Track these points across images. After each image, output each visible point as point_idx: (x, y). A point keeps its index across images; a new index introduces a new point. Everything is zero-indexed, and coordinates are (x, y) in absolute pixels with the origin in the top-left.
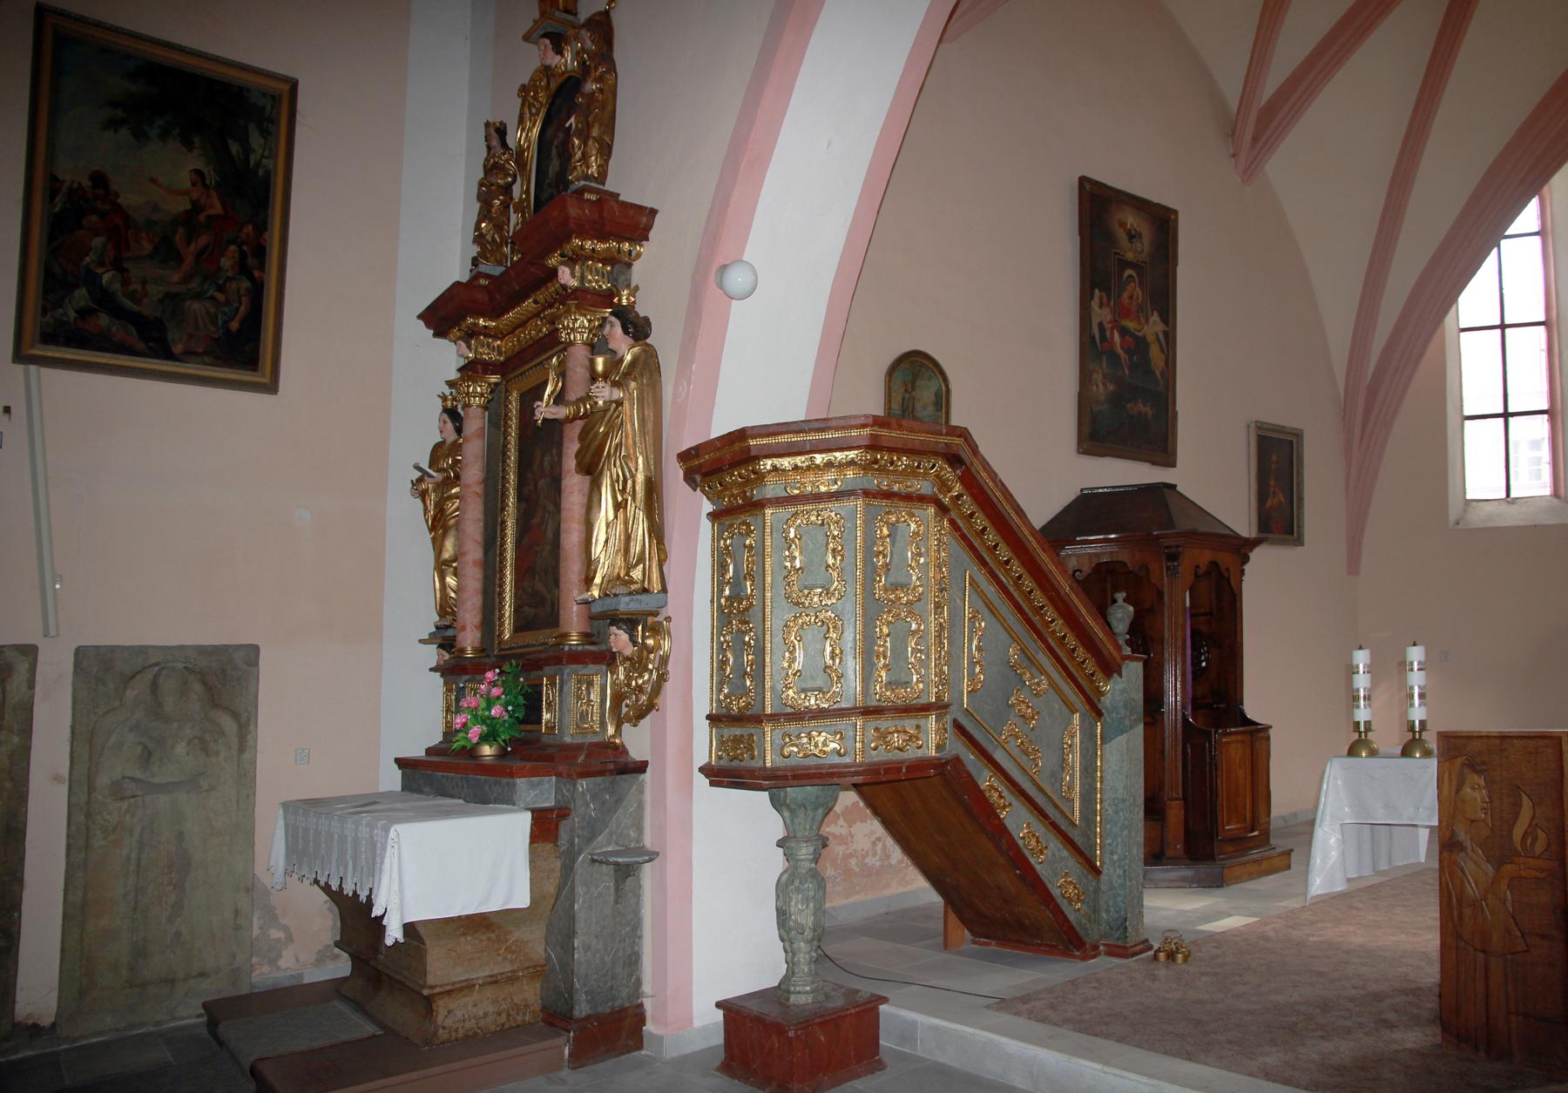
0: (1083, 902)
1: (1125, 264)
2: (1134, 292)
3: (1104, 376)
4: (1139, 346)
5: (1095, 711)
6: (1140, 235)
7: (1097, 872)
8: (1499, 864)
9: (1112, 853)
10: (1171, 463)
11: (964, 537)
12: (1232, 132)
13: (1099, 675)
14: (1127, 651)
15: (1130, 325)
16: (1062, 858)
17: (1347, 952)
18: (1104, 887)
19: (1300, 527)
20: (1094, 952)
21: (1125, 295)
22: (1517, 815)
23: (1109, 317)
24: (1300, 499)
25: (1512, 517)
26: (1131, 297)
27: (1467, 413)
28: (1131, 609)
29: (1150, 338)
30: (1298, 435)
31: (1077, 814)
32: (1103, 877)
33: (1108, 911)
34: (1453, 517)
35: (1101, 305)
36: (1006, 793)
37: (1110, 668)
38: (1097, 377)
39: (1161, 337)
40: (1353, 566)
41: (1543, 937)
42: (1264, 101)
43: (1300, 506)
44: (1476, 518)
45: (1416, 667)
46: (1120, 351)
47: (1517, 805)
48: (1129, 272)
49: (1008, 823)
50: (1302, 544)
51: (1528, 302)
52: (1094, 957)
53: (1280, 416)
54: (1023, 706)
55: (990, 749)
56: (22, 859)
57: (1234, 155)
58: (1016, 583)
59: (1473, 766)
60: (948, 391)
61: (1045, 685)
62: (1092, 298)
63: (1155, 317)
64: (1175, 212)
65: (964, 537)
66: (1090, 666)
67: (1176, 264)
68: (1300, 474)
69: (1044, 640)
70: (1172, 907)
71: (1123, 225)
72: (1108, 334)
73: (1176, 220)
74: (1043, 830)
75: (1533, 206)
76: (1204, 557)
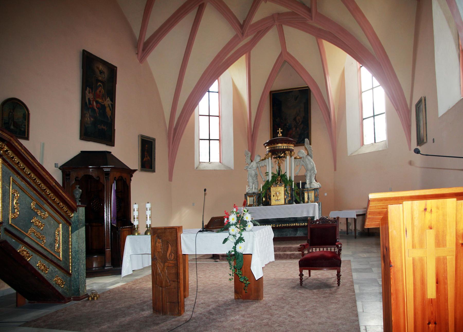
0: (64, 285)
1: (98, 81)
2: (101, 90)
3: (90, 115)
4: (103, 107)
5: (68, 222)
6: (104, 73)
7: (70, 275)
8: (164, 263)
9: (75, 268)
10: (113, 145)
11: (9, 165)
12: (136, 46)
13: (69, 212)
14: (80, 204)
15: (100, 100)
16: (55, 271)
17: (144, 290)
18: (72, 279)
19: (154, 167)
20: (69, 300)
21: (98, 91)
22: (168, 249)
23: (92, 97)
24: (155, 159)
25: (210, 167)
26: (100, 92)
28: (81, 191)
29: (106, 105)
30: (154, 140)
31: (61, 256)
32: (73, 276)
33: (74, 287)
34: (196, 166)
35: (89, 93)
36: (30, 252)
37: (73, 210)
38: (88, 115)
39: (110, 105)
40: (170, 179)
41: (174, 281)
42: (145, 40)
43: (155, 161)
44: (202, 167)
45: (148, 209)
46: (96, 108)
47: (168, 247)
48: (99, 83)
49: (31, 263)
50: (155, 172)
52: (69, 302)
53: (149, 134)
54: (37, 222)
55: (22, 237)
57: (137, 54)
58: (33, 182)
59: (159, 237)
60: (29, 114)
61: (47, 215)
62: (86, 90)
63: (108, 99)
64: (116, 67)
65: (9, 165)
66: (65, 209)
67: (116, 84)
69: (46, 200)
70: (95, 284)
71: (98, 68)
72: (92, 102)
73: (116, 70)
74: (47, 263)
75: (216, 82)
76: (117, 175)
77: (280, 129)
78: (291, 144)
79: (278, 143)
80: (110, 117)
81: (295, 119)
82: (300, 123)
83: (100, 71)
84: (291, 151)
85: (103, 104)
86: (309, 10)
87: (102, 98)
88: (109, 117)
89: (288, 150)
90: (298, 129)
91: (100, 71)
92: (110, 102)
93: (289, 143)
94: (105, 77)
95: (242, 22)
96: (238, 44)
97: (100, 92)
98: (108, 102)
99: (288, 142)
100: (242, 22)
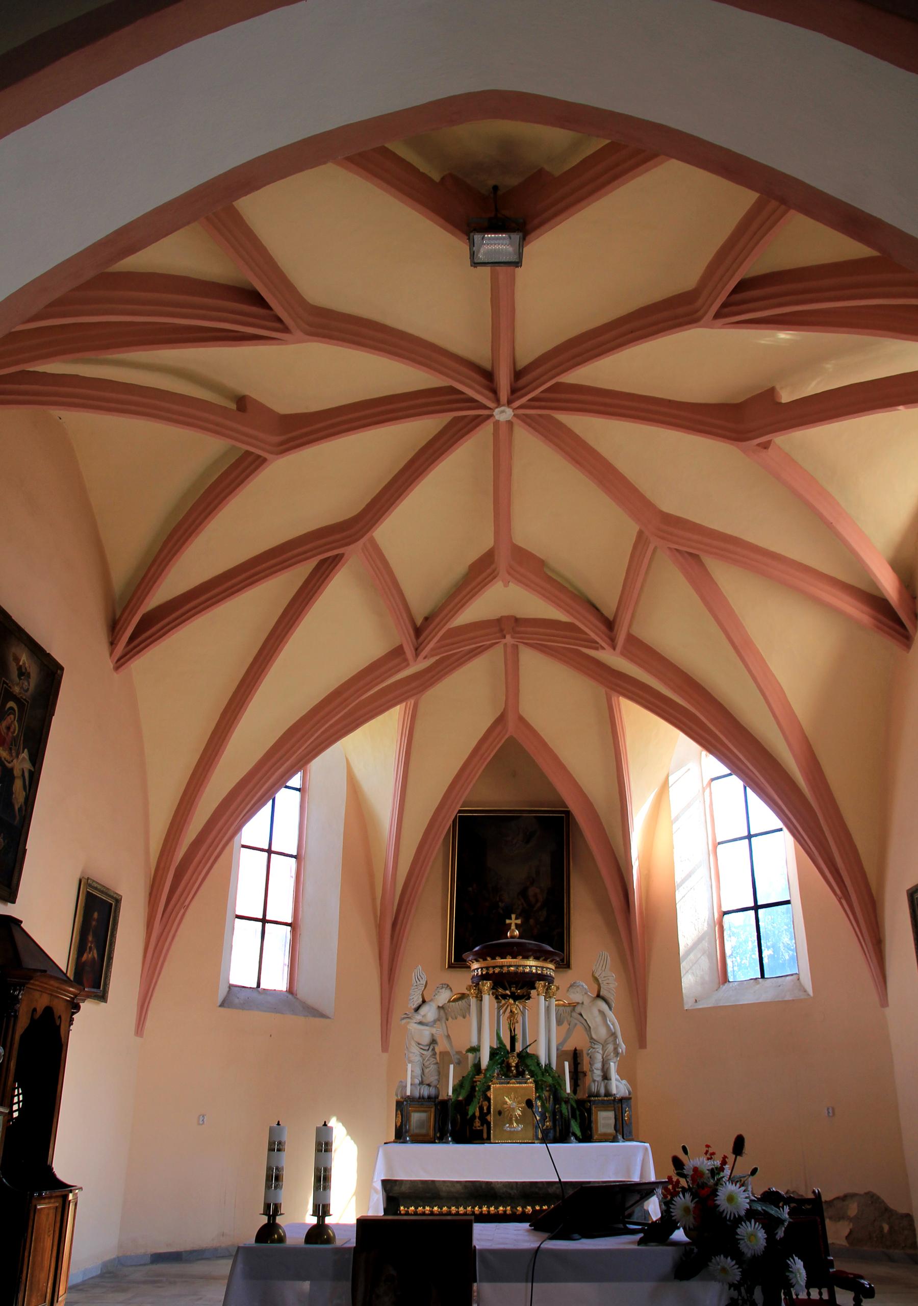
12: (114, 627)
19: (106, 984)
24: (110, 958)
26: (8, 728)
27: (238, 913)
29: (17, 772)
30: (118, 901)
39: (27, 775)
48: (11, 704)
51: (286, 840)
56: (597, 109)
63: (25, 755)
68: (113, 936)
71: (17, 660)
77: (513, 916)
78: (551, 961)
79: (526, 957)
80: (20, 809)
81: (523, 893)
82: (539, 904)
83: (20, 668)
84: (548, 979)
85: (9, 765)
86: (610, 625)
87: (11, 749)
88: (17, 808)
89: (542, 977)
90: (532, 921)
91: (20, 668)
92: (27, 766)
93: (545, 960)
94: (25, 688)
95: (419, 622)
96: (399, 671)
97: (8, 728)
98: (21, 764)
99: (539, 955)
100: (419, 622)
